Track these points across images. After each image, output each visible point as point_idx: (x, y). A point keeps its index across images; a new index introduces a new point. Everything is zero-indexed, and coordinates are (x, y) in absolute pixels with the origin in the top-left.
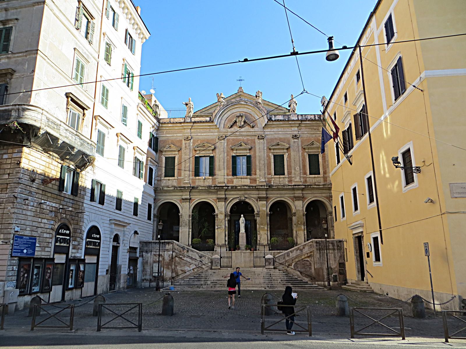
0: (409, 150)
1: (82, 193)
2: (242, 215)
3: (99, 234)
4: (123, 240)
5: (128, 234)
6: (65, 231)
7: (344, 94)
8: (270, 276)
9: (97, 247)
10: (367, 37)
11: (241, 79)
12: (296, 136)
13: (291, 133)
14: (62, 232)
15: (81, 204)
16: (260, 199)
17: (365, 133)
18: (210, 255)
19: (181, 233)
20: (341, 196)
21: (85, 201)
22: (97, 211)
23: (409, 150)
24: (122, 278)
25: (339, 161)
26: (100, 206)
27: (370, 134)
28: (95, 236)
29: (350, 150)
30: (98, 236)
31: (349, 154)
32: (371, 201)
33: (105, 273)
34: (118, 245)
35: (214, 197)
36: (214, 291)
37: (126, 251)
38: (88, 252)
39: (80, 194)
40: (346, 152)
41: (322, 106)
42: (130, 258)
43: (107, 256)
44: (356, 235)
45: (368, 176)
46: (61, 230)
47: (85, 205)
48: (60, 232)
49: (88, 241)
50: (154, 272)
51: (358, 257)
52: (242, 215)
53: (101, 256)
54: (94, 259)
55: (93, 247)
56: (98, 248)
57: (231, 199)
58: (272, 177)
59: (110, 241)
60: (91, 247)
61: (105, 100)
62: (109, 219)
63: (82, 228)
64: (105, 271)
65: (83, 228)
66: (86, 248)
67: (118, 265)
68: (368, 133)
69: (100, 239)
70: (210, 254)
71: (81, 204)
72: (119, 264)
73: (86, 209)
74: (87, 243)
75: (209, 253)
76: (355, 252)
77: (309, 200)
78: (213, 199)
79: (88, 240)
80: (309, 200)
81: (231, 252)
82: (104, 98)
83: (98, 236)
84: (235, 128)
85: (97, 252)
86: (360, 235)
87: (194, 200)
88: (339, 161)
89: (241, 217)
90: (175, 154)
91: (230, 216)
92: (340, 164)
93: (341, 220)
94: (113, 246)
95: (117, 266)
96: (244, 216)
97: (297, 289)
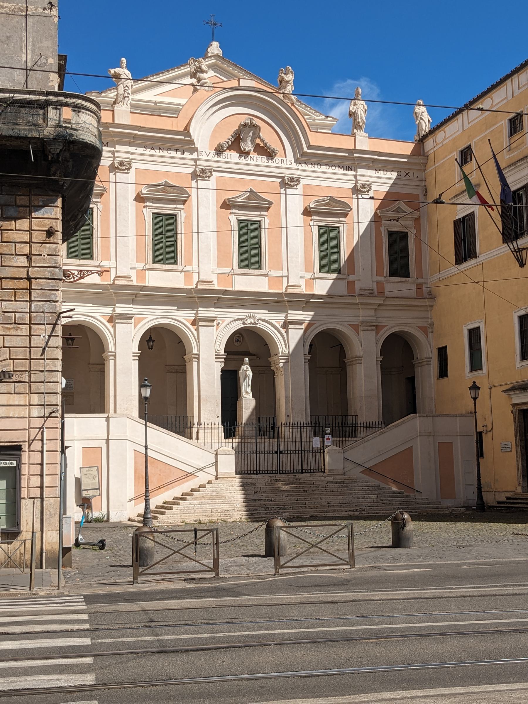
35: (190, 315)
50: (83, 488)
51: (523, 448)
58: (316, 275)
77: (317, 327)
78: (185, 319)
80: (317, 327)
89: (242, 363)
90: (176, 209)
96: (250, 364)
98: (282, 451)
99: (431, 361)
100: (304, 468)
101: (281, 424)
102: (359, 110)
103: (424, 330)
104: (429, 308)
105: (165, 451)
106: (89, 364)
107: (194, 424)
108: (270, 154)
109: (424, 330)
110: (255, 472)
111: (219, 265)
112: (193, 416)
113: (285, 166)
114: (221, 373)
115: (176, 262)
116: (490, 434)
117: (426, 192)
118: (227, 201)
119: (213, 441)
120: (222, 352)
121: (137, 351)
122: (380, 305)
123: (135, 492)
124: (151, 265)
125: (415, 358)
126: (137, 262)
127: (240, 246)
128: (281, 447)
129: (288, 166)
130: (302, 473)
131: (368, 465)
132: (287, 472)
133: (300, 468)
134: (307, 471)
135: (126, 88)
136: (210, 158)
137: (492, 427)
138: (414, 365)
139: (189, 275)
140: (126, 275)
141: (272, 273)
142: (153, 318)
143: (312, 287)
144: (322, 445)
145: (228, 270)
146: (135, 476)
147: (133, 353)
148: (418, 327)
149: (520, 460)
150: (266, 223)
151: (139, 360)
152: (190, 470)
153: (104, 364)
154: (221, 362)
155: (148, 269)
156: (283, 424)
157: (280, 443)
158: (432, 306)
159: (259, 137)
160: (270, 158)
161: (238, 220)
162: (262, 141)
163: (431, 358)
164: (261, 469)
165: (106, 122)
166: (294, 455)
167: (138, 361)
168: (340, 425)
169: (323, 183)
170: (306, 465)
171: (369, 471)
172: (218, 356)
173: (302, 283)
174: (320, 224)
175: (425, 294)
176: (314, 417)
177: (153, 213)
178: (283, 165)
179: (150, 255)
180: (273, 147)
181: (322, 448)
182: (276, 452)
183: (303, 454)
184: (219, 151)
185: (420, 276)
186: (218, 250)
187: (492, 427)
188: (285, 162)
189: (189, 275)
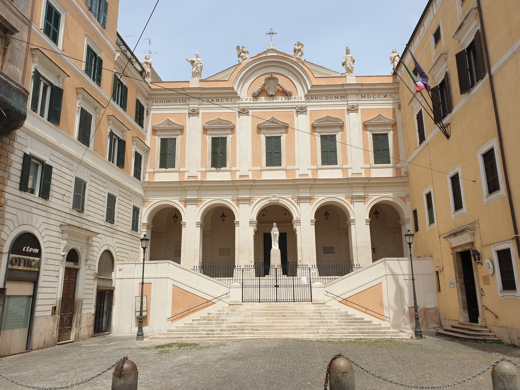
2: (275, 224)
3: (39, 247)
4: (86, 260)
5: (98, 251)
6: (31, 249)
8: (321, 316)
9: (33, 269)
11: (273, 31)
12: (353, 107)
13: (237, 106)
14: (27, 251)
16: (300, 200)
18: (226, 283)
20: (427, 191)
25: (422, 138)
27: (491, 77)
29: (445, 116)
30: (36, 251)
31: (445, 121)
33: (50, 313)
34: (76, 267)
40: (438, 118)
41: (392, 63)
42: (99, 288)
43: (54, 285)
44: (460, 250)
45: (485, 149)
46: (25, 248)
47: (7, 196)
48: (24, 250)
49: (13, 258)
51: (462, 284)
52: (275, 224)
53: (41, 283)
54: (26, 289)
55: (26, 268)
56: (37, 270)
57: (259, 199)
60: (21, 268)
62: (59, 224)
64: (50, 308)
67: (77, 298)
68: (487, 76)
69: (39, 255)
70: (226, 281)
72: (78, 297)
73: (9, 203)
74: (10, 262)
76: (457, 275)
78: (398, 197)
79: (12, 256)
82: (52, 28)
83: (36, 251)
84: (263, 99)
86: (467, 248)
87: (205, 201)
88: (422, 138)
89: (272, 226)
91: (257, 226)
94: (67, 269)
95: (76, 300)
96: (277, 226)
97: (366, 336)
98: (278, 286)
99: (409, 221)
100: (295, 298)
102: (348, 60)
103: (404, 199)
104: (406, 184)
106: (388, 228)
108: (287, 94)
109: (404, 199)
110: (258, 301)
111: (253, 165)
113: (297, 100)
114: (254, 233)
115: (336, 164)
116: (442, 273)
117: (400, 106)
118: (364, 123)
120: (255, 220)
121: (314, 219)
123: (172, 314)
124: (158, 169)
125: (401, 219)
126: (201, 167)
128: (278, 283)
129: (299, 100)
131: (344, 297)
132: (284, 301)
133: (276, 299)
135: (197, 68)
137: (443, 267)
138: (401, 225)
139: (345, 170)
140: (306, 174)
141: (288, 168)
145: (259, 168)
147: (196, 222)
149: (460, 294)
152: (209, 298)
153: (348, 229)
154: (253, 226)
155: (209, 171)
156: (250, 266)
158: (408, 182)
159: (279, 85)
160: (287, 97)
162: (281, 87)
164: (280, 299)
165: (182, 87)
166: (288, 288)
167: (314, 226)
168: (227, 268)
169: (324, 108)
170: (280, 297)
171: (346, 301)
172: (251, 223)
175: (403, 175)
176: (204, 263)
177: (212, 138)
178: (295, 100)
179: (209, 162)
181: (309, 284)
182: (278, 286)
183: (261, 288)
184: (256, 96)
185: (345, 161)
187: (443, 267)
188: (297, 98)
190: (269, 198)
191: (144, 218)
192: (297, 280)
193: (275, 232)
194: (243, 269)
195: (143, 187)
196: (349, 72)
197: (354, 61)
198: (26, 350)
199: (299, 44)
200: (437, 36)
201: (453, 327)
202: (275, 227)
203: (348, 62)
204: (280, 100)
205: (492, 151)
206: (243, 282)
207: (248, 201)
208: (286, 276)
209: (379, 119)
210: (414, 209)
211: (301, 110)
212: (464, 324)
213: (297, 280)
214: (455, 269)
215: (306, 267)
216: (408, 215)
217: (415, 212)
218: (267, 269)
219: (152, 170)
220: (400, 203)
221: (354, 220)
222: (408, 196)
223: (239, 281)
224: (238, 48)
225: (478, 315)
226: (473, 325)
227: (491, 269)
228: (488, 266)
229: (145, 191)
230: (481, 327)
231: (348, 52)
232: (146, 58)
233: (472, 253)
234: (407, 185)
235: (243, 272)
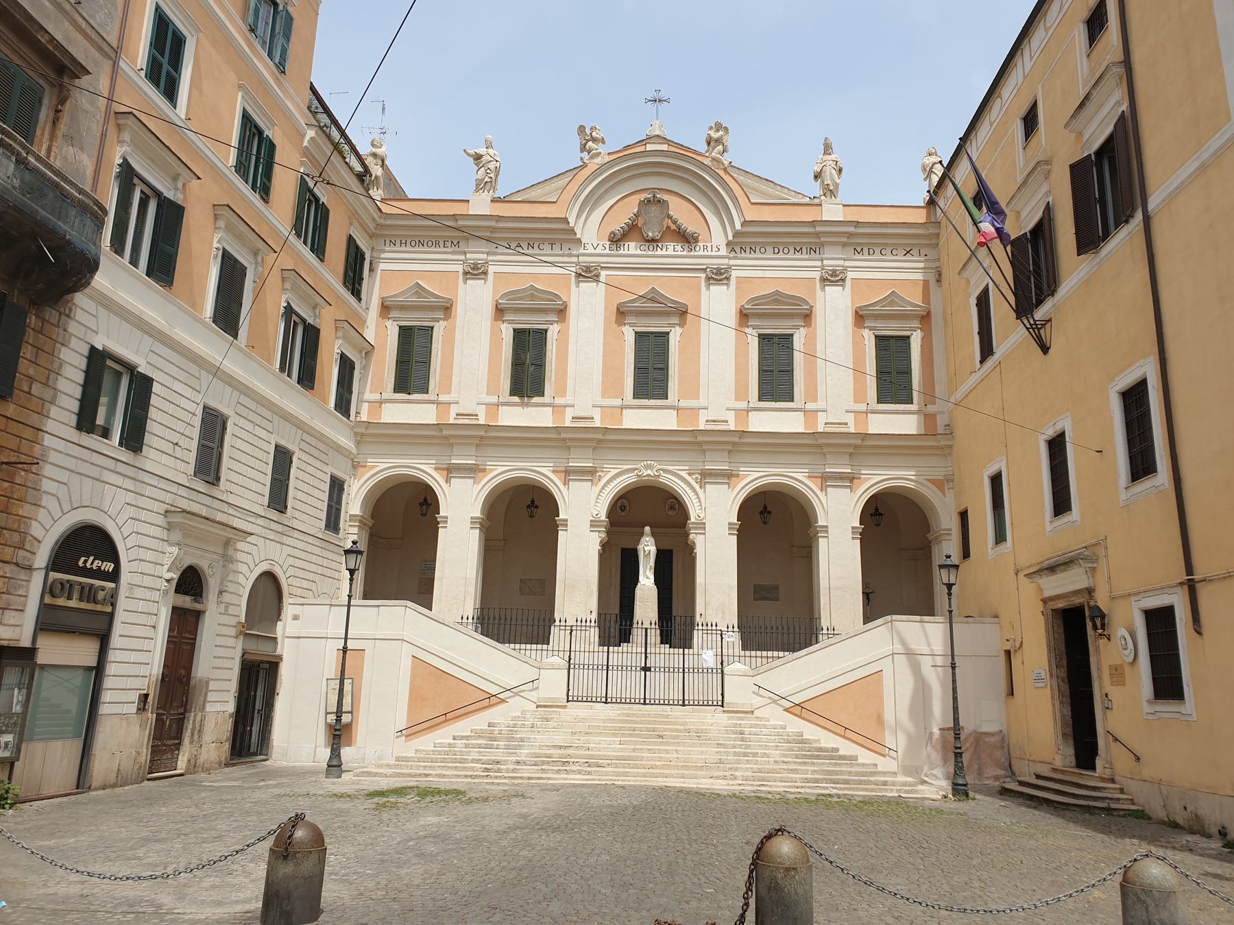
0: (1062, 435)
1: (34, 391)
2: (647, 529)
3: (115, 559)
6: (97, 563)
7: (1024, 109)
8: (742, 740)
9: (99, 608)
10: (992, 120)
11: (663, 95)
14: (88, 565)
15: (28, 433)
16: (706, 477)
17: (1123, 218)
19: (442, 579)
20: (992, 470)
21: (50, 426)
22: (105, 472)
23: (1062, 435)
24: (209, 726)
25: (987, 350)
26: (124, 455)
27: (1147, 219)
28: (93, 563)
29: (1040, 302)
30: (109, 567)
31: (1039, 314)
32: (1141, 465)
33: (133, 708)
34: (198, 606)
36: (538, 785)
37: (233, 632)
38: (50, 621)
39: (29, 393)
40: (1024, 307)
41: (925, 179)
42: (246, 656)
43: (146, 645)
45: (1127, 380)
46: (83, 559)
47: (48, 440)
48: (81, 563)
49: (55, 581)
51: (1063, 681)
52: (647, 529)
54: (82, 652)
55: (83, 605)
56: (109, 609)
57: (614, 472)
59: (166, 592)
60: (73, 603)
61: (166, 67)
63: (29, 527)
64: (134, 696)
65: (35, 530)
66: (44, 608)
69: (114, 576)
71: (28, 433)
72: (199, 675)
73: (53, 457)
74: (50, 589)
75: (523, 652)
76: (1053, 662)
81: (606, 648)
83: (109, 567)
84: (632, 247)
85: (100, 625)
86: (1077, 601)
87: (493, 470)
88: (987, 350)
89: (642, 534)
91: (608, 532)
92: (990, 362)
93: (990, 552)
94: (176, 611)
96: (653, 534)
99: (950, 534)
100: (686, 698)
101: (651, 624)
103: (940, 485)
105: (460, 660)
107: (822, 629)
108: (687, 238)
109: (940, 485)
110: (604, 700)
112: (820, 618)
113: (710, 253)
117: (940, 275)
119: (591, 650)
120: (603, 518)
122: (856, 447)
127: (762, 371)
128: (648, 661)
129: (714, 253)
130: (645, 703)
131: (797, 699)
133: (604, 695)
134: (652, 702)
135: (488, 171)
136: (598, 251)
138: (930, 542)
139: (810, 415)
141: (683, 403)
142: (878, 480)
143: (496, 417)
144: (719, 662)
146: (410, 696)
147: (472, 518)
148: (928, 480)
149: (1057, 703)
150: (553, 332)
151: (861, 539)
152: (493, 690)
154: (599, 531)
155: (504, 404)
157: (648, 655)
159: (669, 217)
160: (687, 245)
161: (636, 333)
162: (675, 222)
163: (951, 530)
168: (536, 622)
169: (768, 274)
171: (799, 709)
172: (594, 524)
173: (731, 416)
174: (878, 333)
175: (940, 430)
176: (603, 616)
178: (706, 253)
179: (505, 383)
180: (690, 229)
181: (719, 666)
185: (812, 395)
186: (605, 375)
188: (709, 249)
189: (810, 415)
190: (637, 469)
191: (354, 503)
192: (691, 657)
193: (648, 547)
194: (572, 626)
195: (356, 434)
196: (828, 194)
197: (841, 170)
198: (77, 788)
199: (719, 127)
200: (1030, 121)
201: (1038, 777)
202: (647, 536)
203: (828, 173)
204: (672, 249)
205: (1142, 384)
206: (570, 656)
207: (590, 474)
208: (667, 646)
209: (892, 303)
210: (962, 508)
211: (718, 276)
212: (1063, 772)
213: (691, 657)
214: (1049, 646)
215: (714, 628)
216: (947, 521)
217: (964, 515)
218: (667, 631)
219: (377, 397)
220: (931, 494)
221: (827, 527)
222: (949, 479)
223: (561, 654)
224: (581, 129)
225: (1097, 754)
226: (1083, 775)
227: (1129, 650)
228: (1123, 642)
229: (358, 444)
230: (1102, 779)
231: (827, 149)
232: (373, 145)
233: (1087, 613)
234: (950, 454)
235: (571, 634)
